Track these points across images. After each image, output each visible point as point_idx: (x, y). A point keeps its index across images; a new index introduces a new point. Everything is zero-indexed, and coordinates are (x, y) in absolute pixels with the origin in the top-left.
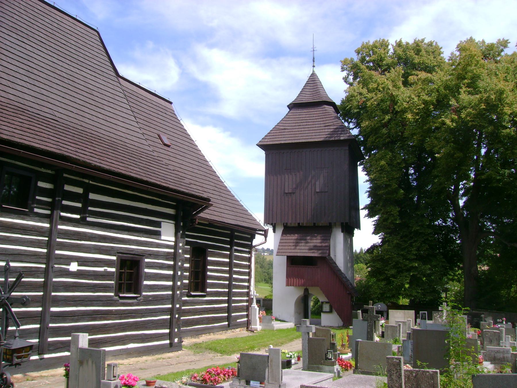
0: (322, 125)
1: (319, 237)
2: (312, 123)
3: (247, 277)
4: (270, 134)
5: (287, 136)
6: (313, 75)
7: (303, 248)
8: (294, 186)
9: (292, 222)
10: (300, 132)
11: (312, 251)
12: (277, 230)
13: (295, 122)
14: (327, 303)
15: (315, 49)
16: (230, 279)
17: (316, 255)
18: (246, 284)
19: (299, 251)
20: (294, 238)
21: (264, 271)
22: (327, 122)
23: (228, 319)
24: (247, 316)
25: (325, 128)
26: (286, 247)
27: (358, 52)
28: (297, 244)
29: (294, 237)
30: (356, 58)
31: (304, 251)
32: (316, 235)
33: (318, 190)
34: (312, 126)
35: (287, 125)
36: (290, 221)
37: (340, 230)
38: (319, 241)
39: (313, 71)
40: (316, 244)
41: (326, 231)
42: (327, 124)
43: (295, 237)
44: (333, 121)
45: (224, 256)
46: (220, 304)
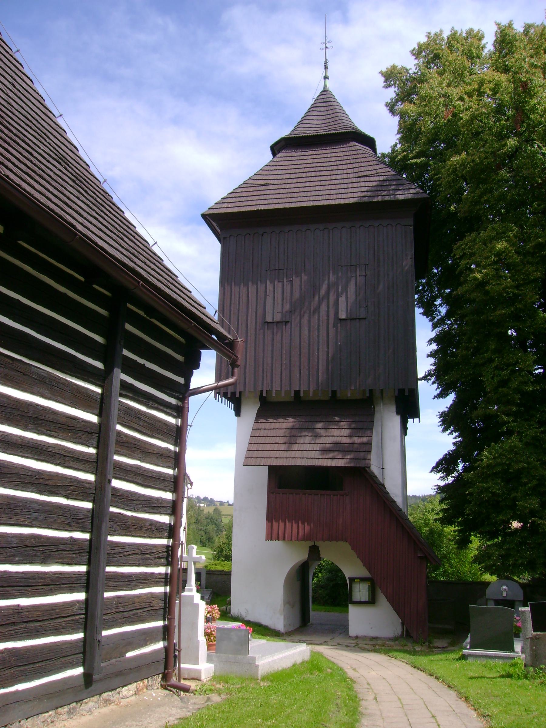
0: (351, 176)
1: (343, 424)
2: (328, 173)
3: (168, 496)
4: (233, 195)
5: (271, 197)
6: (325, 91)
7: (308, 447)
8: (287, 307)
9: (279, 388)
10: (301, 190)
11: (331, 455)
12: (244, 410)
13: (289, 171)
14: (363, 580)
15: (328, 45)
16: (98, 493)
17: (341, 463)
18: (165, 519)
19: (298, 454)
20: (285, 425)
21: (200, 527)
22: (363, 169)
23: (85, 652)
24: (166, 633)
25: (358, 180)
26: (268, 447)
27: (417, 53)
28: (291, 438)
29: (285, 424)
30: (411, 64)
31: (312, 454)
32: (337, 419)
33: (342, 315)
34: (329, 178)
35: (271, 177)
36: (276, 387)
37: (393, 408)
38: (346, 432)
39: (325, 86)
40: (339, 439)
41: (359, 410)
42: (363, 174)
43: (289, 423)
44: (376, 167)
45: (154, 529)
46: (50, 593)
